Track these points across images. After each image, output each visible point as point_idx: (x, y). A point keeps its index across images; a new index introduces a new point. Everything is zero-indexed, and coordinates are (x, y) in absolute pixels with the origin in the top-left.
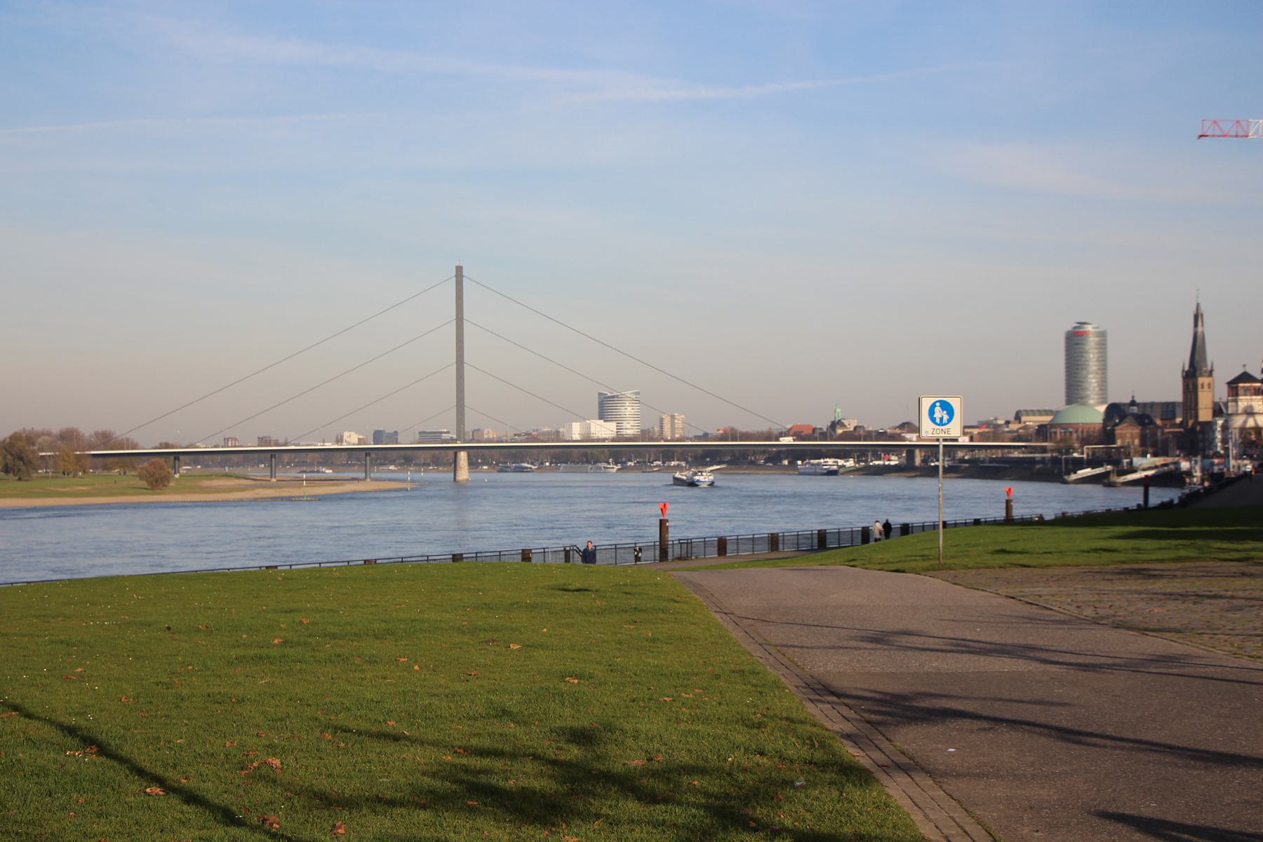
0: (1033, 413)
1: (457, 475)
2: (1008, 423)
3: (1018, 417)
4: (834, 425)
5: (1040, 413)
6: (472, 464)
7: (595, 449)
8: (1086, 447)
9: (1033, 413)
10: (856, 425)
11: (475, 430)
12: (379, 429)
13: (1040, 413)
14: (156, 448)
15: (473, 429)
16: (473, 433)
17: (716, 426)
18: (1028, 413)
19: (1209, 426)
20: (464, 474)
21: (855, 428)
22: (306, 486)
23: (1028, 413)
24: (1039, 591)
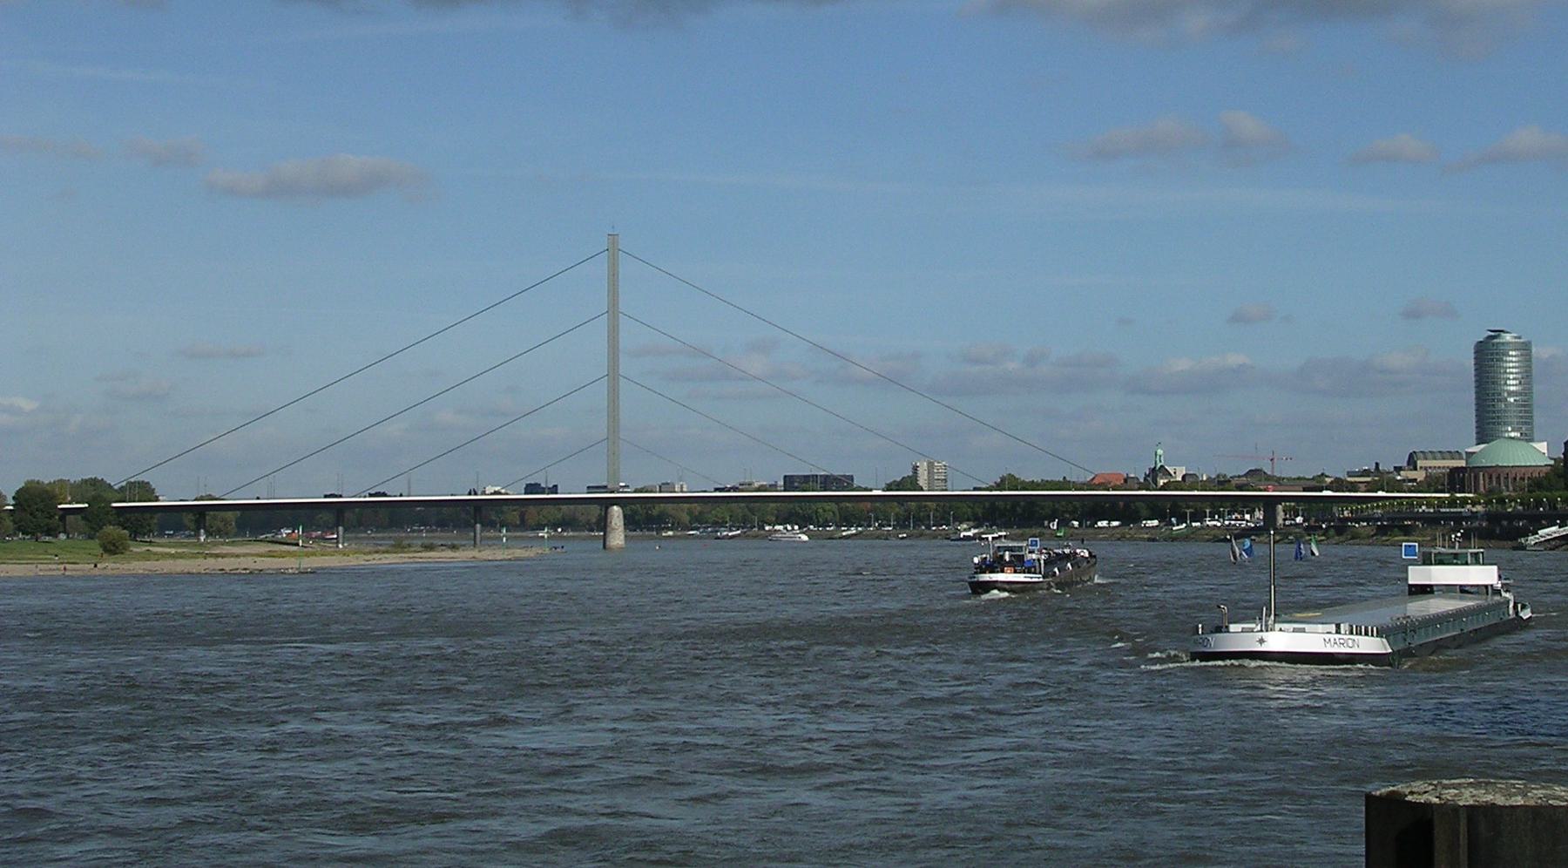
0: (1433, 455)
1: (608, 539)
2: (1398, 469)
3: (1412, 462)
4: (1154, 473)
5: (1443, 455)
6: (631, 522)
7: (724, 506)
8: (1512, 598)
9: (1433, 455)
10: (1184, 473)
11: (663, 484)
12: (18, 489)
13: (1443, 455)
14: (196, 500)
15: (660, 483)
16: (660, 487)
17: (1235, 469)
18: (1425, 456)
19: (1537, 534)
20: (617, 537)
21: (1184, 477)
22: (338, 535)
23: (1425, 456)
24: (23, 804)
